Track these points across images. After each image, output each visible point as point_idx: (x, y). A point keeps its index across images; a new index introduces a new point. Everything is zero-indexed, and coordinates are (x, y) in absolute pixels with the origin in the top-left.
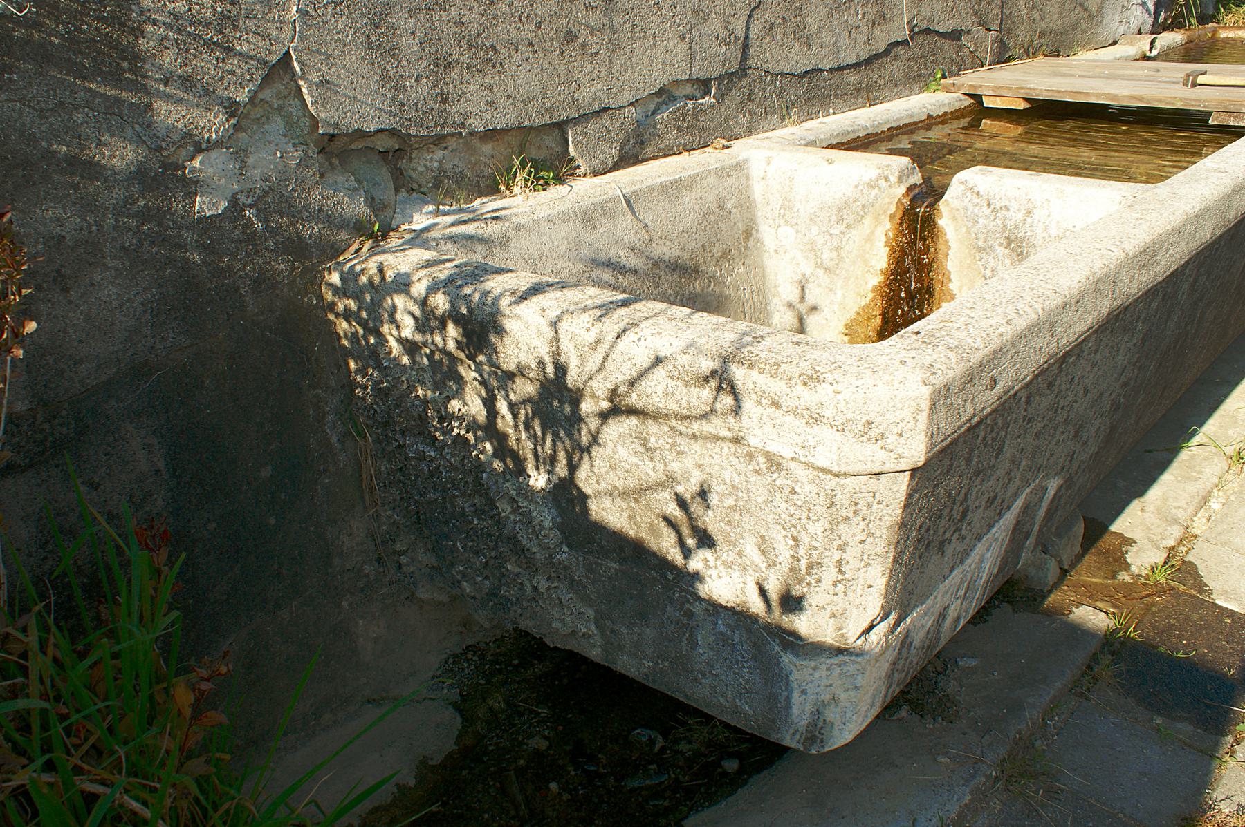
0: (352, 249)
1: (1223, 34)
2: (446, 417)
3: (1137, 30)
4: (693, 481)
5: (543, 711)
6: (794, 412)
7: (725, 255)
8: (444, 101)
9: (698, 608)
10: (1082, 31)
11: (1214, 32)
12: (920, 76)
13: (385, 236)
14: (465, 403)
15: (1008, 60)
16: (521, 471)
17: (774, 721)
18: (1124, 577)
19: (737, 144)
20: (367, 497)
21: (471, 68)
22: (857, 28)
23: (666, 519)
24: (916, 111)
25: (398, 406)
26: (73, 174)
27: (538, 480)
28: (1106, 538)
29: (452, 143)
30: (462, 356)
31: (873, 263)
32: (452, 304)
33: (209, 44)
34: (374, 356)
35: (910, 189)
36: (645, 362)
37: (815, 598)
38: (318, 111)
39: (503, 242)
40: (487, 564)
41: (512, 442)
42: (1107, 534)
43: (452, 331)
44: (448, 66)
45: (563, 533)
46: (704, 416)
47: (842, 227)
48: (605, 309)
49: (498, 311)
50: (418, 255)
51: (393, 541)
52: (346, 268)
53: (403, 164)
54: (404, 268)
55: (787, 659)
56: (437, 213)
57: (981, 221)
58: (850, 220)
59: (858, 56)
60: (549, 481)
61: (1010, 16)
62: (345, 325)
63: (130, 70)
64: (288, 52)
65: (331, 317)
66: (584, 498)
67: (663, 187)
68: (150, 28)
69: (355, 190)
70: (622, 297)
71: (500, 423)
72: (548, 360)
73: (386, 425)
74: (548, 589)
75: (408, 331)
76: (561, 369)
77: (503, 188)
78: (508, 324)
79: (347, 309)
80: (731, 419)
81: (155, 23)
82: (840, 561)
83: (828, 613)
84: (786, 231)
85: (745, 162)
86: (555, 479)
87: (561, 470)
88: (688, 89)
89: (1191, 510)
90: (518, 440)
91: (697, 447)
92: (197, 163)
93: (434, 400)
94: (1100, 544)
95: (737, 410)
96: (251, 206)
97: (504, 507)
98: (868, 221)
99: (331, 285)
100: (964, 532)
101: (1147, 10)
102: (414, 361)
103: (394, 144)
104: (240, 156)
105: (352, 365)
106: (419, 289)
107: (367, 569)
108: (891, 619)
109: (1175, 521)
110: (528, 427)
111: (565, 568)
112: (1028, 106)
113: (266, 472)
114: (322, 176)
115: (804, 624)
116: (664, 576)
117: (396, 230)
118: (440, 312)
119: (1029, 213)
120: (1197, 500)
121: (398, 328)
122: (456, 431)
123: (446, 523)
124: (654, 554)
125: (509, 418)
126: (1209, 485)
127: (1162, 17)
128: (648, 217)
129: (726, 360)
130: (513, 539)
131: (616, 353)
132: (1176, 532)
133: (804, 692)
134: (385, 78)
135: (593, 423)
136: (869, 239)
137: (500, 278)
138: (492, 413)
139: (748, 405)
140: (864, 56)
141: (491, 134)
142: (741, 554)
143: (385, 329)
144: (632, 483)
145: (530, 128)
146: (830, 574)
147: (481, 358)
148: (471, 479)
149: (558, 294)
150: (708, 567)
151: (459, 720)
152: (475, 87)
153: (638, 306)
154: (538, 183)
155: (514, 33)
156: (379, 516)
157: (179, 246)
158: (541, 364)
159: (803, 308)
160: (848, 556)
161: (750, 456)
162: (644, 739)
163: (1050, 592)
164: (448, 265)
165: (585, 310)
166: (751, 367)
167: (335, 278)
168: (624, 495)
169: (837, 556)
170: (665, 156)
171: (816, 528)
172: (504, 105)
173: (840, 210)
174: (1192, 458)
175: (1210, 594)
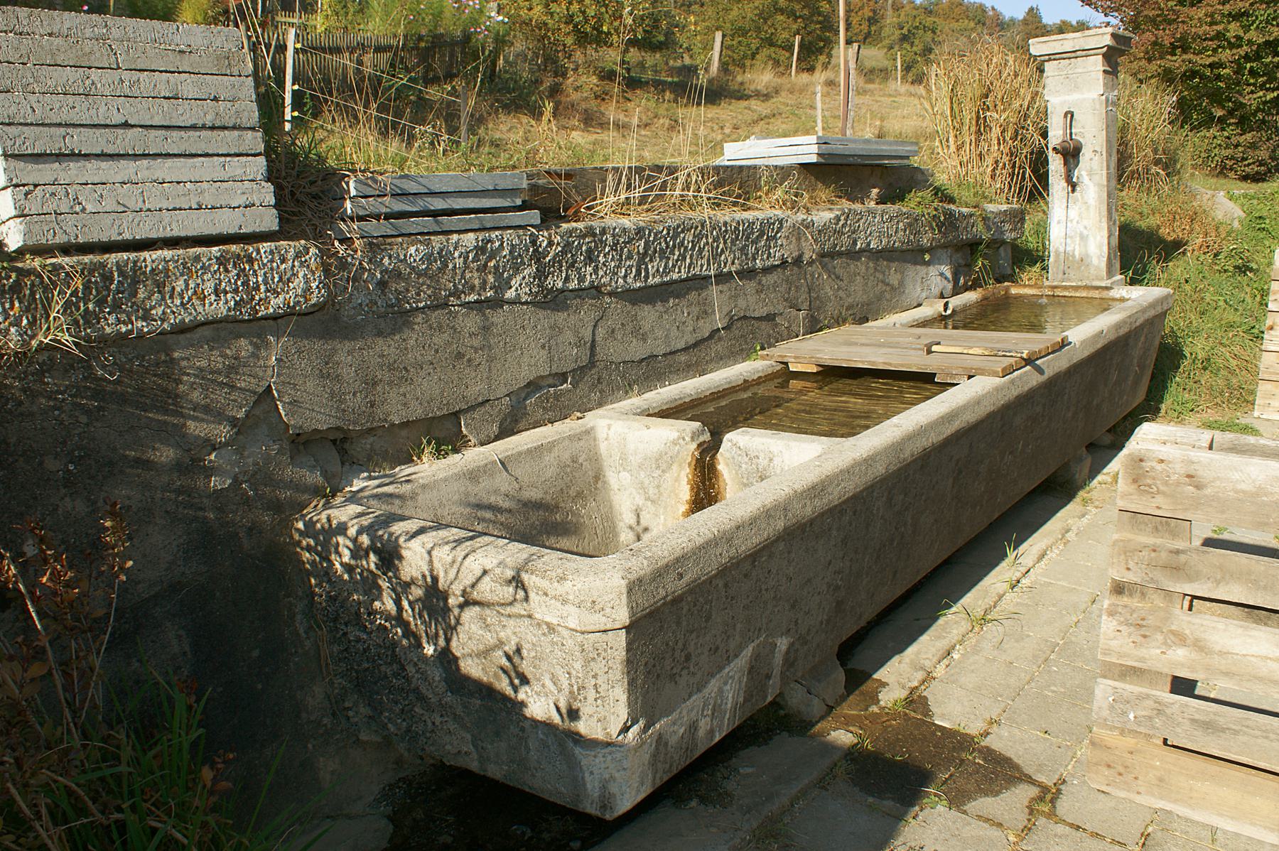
0: (312, 505)
1: (1014, 291)
2: (372, 613)
3: (938, 294)
4: (513, 643)
5: (451, 819)
6: (555, 597)
7: (580, 495)
8: (372, 406)
9: (527, 724)
10: (887, 300)
11: (1007, 289)
12: (742, 350)
13: (334, 496)
14: (384, 604)
15: (821, 330)
16: (420, 646)
17: (578, 795)
18: (874, 709)
19: (589, 415)
20: (324, 669)
21: (390, 383)
22: (684, 323)
23: (502, 669)
24: (733, 379)
25: (342, 607)
26: (137, 468)
27: (429, 650)
28: (869, 683)
29: (380, 432)
30: (379, 573)
31: (681, 496)
32: (372, 540)
34: (327, 574)
35: (699, 445)
36: (479, 573)
37: (586, 710)
38: (289, 420)
39: (414, 496)
40: (403, 710)
41: (413, 627)
42: (870, 681)
43: (373, 557)
44: (375, 384)
45: (447, 683)
46: (511, 604)
47: (659, 472)
48: (459, 542)
49: (399, 546)
50: (354, 509)
51: (344, 701)
52: (307, 519)
53: (347, 446)
54: (344, 519)
55: (578, 750)
56: (370, 478)
57: (744, 466)
58: (664, 466)
59: (686, 343)
60: (435, 650)
61: (818, 298)
62: (307, 555)
63: (173, 404)
64: (270, 386)
65: (298, 550)
66: (456, 659)
67: (529, 451)
68: (185, 378)
69: (315, 466)
70: (471, 534)
71: (405, 614)
72: (427, 573)
73: (335, 620)
74: (441, 723)
75: (346, 559)
76: (435, 579)
77: (415, 458)
78: (404, 553)
79: (308, 545)
80: (525, 604)
81: (188, 375)
82: (595, 685)
83: (595, 719)
84: (624, 475)
85: (592, 428)
86: (439, 648)
87: (442, 642)
88: (551, 381)
89: (935, 660)
90: (416, 625)
91: (512, 622)
92: (213, 457)
93: (364, 602)
94: (863, 688)
95: (527, 599)
96: (246, 482)
97: (411, 670)
98: (675, 467)
99: (298, 530)
100: (692, 669)
101: (946, 278)
102: (351, 577)
103: (340, 435)
104: (240, 451)
105: (313, 581)
106: (352, 532)
107: (325, 720)
108: (641, 723)
109: (922, 668)
110: (421, 616)
111: (451, 707)
112: (821, 369)
113: (256, 653)
114: (292, 458)
115: (582, 727)
116: (505, 705)
117: (341, 491)
118: (365, 546)
119: (771, 460)
120: (941, 652)
121: (340, 556)
122: (378, 621)
123: (376, 683)
124: (499, 692)
125: (410, 611)
126: (954, 641)
127: (962, 281)
128: (518, 472)
129: (518, 571)
130: (416, 690)
131: (463, 569)
132: (920, 675)
133: (592, 773)
134: (332, 395)
135: (456, 611)
136: (677, 480)
137: (401, 524)
138: (400, 608)
139: (532, 595)
140: (692, 341)
141: (406, 424)
142: (543, 686)
143: (333, 557)
144: (481, 647)
145: (433, 418)
146: (591, 694)
147: (390, 574)
148: (389, 653)
149: (435, 533)
150: (528, 697)
151: (391, 827)
152: (393, 395)
153: (478, 540)
154: (439, 453)
155: (419, 358)
156: (333, 683)
157: (201, 509)
158: (424, 576)
159: (640, 529)
160: (599, 682)
161: (539, 625)
162: (519, 832)
163: (817, 722)
164: (371, 516)
165: (447, 543)
166: (532, 574)
167: (300, 525)
168: (478, 655)
169: (593, 681)
170: (534, 428)
171: (578, 665)
172: (413, 404)
173: (657, 460)
174: (947, 623)
175: (931, 717)
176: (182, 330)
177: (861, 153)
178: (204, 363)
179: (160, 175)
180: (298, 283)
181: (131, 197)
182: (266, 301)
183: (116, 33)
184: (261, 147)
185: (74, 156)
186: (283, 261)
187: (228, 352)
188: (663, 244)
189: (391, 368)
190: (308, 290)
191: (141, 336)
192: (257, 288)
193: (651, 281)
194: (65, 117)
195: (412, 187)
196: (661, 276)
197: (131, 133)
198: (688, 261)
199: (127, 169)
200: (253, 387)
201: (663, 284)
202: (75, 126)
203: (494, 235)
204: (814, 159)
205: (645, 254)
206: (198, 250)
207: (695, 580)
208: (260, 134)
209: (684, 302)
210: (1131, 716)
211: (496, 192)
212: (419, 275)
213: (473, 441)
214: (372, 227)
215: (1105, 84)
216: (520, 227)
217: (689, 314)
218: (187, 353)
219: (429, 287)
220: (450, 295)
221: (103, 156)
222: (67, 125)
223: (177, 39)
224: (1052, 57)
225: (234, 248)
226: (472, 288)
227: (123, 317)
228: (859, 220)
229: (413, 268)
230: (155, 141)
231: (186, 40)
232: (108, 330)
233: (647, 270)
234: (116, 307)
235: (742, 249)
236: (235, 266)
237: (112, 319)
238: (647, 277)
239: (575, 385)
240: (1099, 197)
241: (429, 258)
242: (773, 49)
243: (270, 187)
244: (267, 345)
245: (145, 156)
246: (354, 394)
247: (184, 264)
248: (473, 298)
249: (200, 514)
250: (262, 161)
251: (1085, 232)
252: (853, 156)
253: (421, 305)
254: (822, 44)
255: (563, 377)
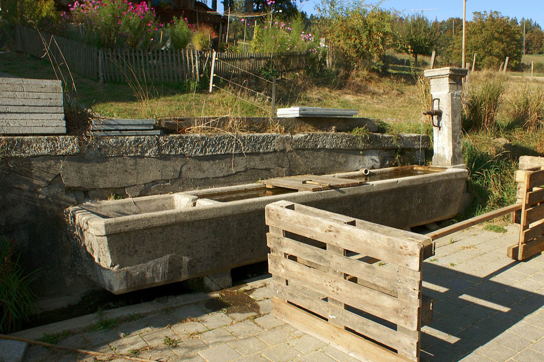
21: (100, 176)
29: (97, 190)
33: (45, 172)
44: (95, 176)
64: (60, 173)
88: (163, 182)
104: (49, 189)
113: (49, 244)
128: (140, 206)
134: (80, 177)
157: (36, 203)
170: (154, 195)
176: (34, 156)
177: (324, 113)
178: (40, 166)
179: (32, 118)
180: (71, 147)
181: (23, 123)
182: (60, 151)
183: (25, 83)
184: (63, 111)
185: (8, 113)
186: (66, 141)
187: (48, 163)
188: (214, 143)
189: (101, 172)
190: (73, 149)
191: (22, 157)
192: (58, 147)
193: (207, 154)
194: (7, 103)
195: (113, 123)
196: (212, 153)
197: (25, 107)
198: (225, 148)
199: (23, 116)
200: (54, 173)
201: (213, 155)
202: (9, 105)
203: (141, 137)
204: (298, 116)
205: (205, 145)
206: (41, 137)
207: (133, 228)
208: (63, 108)
209: (223, 162)
210: (277, 292)
211: (143, 125)
212: (113, 147)
213: (130, 196)
214: (98, 133)
215: (450, 89)
216: (152, 135)
217: (225, 166)
218: (35, 162)
219: (116, 151)
220: (124, 153)
221: (17, 113)
222: (8, 105)
223: (42, 84)
224: (432, 77)
225: (52, 137)
226: (132, 152)
227: (17, 152)
228: (318, 138)
229: (111, 145)
230: (32, 109)
231: (45, 84)
232: (13, 155)
233: (206, 150)
234: (16, 150)
235: (253, 146)
236: (51, 141)
237: (14, 152)
238: (206, 152)
239: (172, 184)
240: (448, 132)
241: (117, 143)
242: (491, 57)
243: (65, 122)
244: (60, 163)
245: (28, 113)
246: (87, 178)
247: (36, 140)
248: (133, 155)
249: (35, 204)
250: (63, 115)
251: (444, 146)
252: (319, 115)
253: (113, 156)
254: (516, 55)
255: (168, 181)
